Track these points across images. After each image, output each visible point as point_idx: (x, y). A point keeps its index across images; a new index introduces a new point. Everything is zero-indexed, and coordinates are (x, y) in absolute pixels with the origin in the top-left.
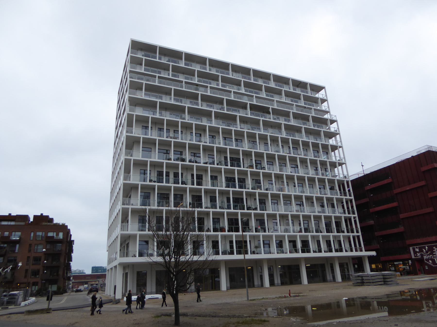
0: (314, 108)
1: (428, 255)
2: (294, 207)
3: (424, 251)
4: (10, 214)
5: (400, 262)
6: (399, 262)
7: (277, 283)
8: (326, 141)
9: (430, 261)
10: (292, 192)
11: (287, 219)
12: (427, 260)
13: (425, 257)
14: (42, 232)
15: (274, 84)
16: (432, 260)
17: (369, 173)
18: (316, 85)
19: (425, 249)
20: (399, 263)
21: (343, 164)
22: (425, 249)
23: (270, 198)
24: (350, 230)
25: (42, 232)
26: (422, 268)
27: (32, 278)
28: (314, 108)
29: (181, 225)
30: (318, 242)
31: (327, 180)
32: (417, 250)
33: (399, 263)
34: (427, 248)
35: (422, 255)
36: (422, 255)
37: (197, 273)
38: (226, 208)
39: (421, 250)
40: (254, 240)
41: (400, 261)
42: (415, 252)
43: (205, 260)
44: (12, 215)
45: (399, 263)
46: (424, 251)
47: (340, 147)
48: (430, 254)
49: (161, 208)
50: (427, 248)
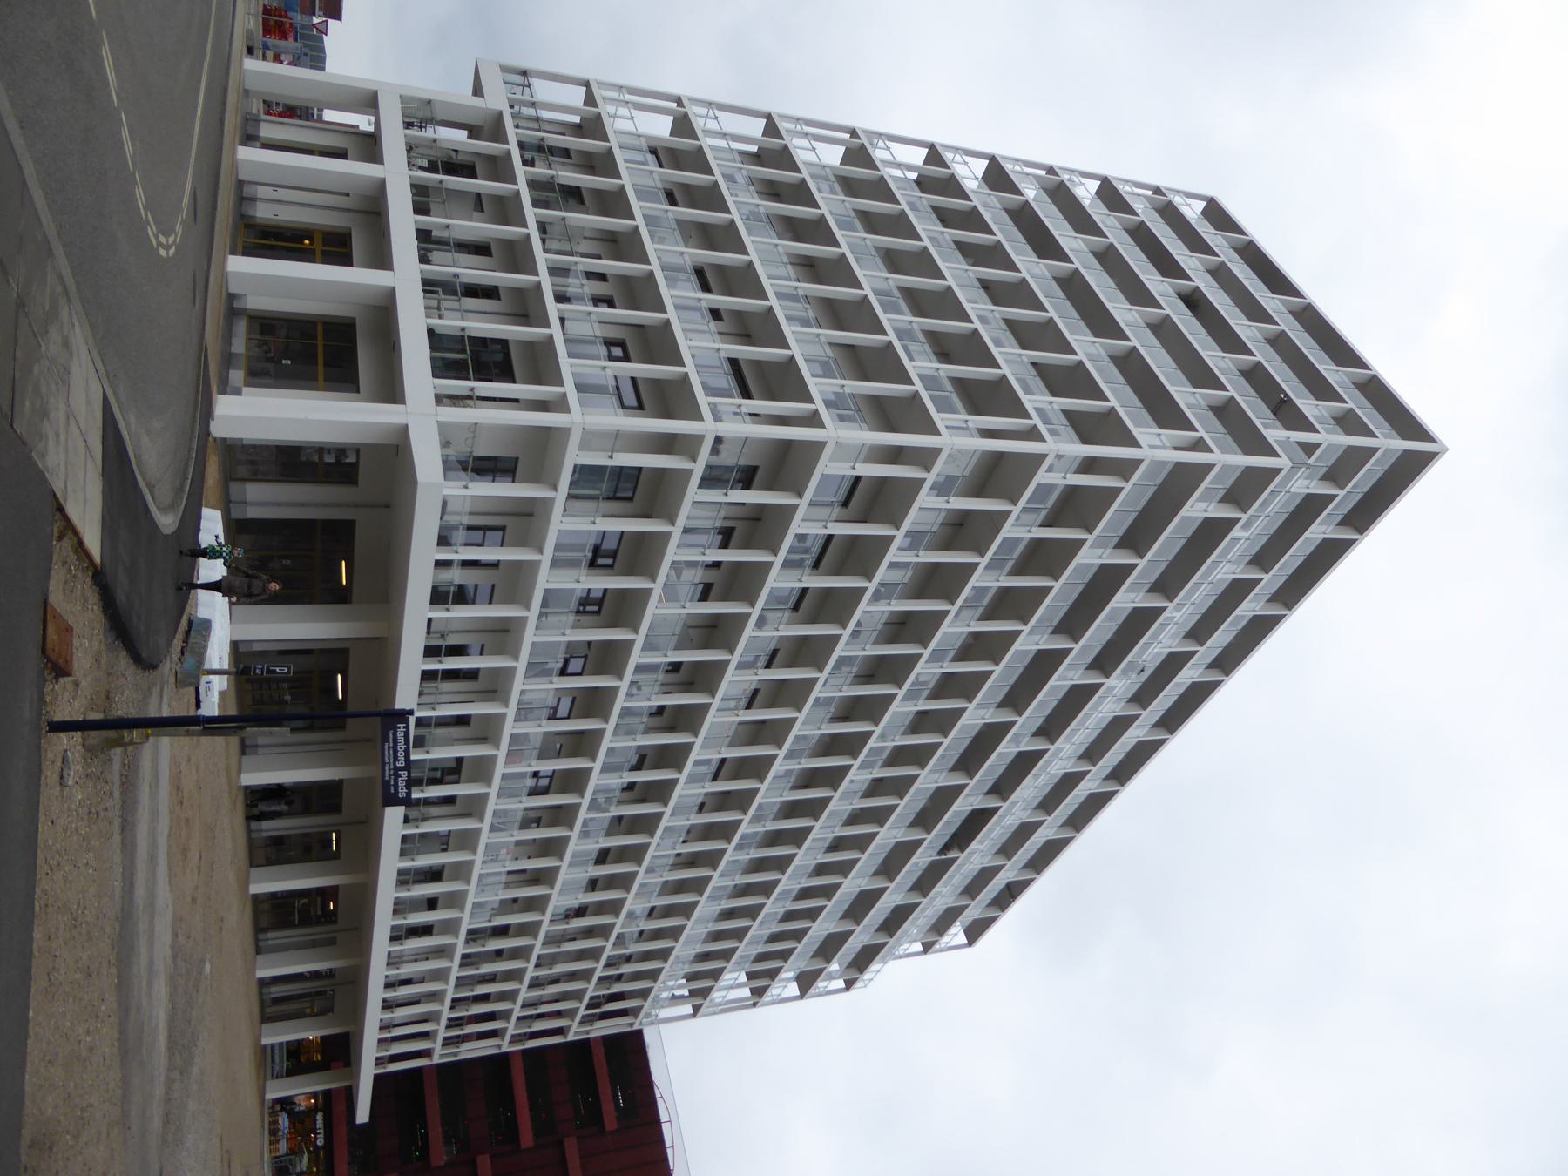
0: (772, 563)
2: (622, 780)
5: (322, 1136)
6: (322, 1131)
7: (260, 741)
8: (472, 634)
10: (722, 699)
11: (485, 649)
15: (530, 136)
18: (1332, 569)
20: (318, 1131)
26: (194, 455)
27: (274, 1123)
28: (772, 563)
29: (164, 894)
31: (546, 895)
33: (319, 1134)
40: (348, 210)
41: (325, 1139)
45: (319, 1134)
47: (696, 1009)
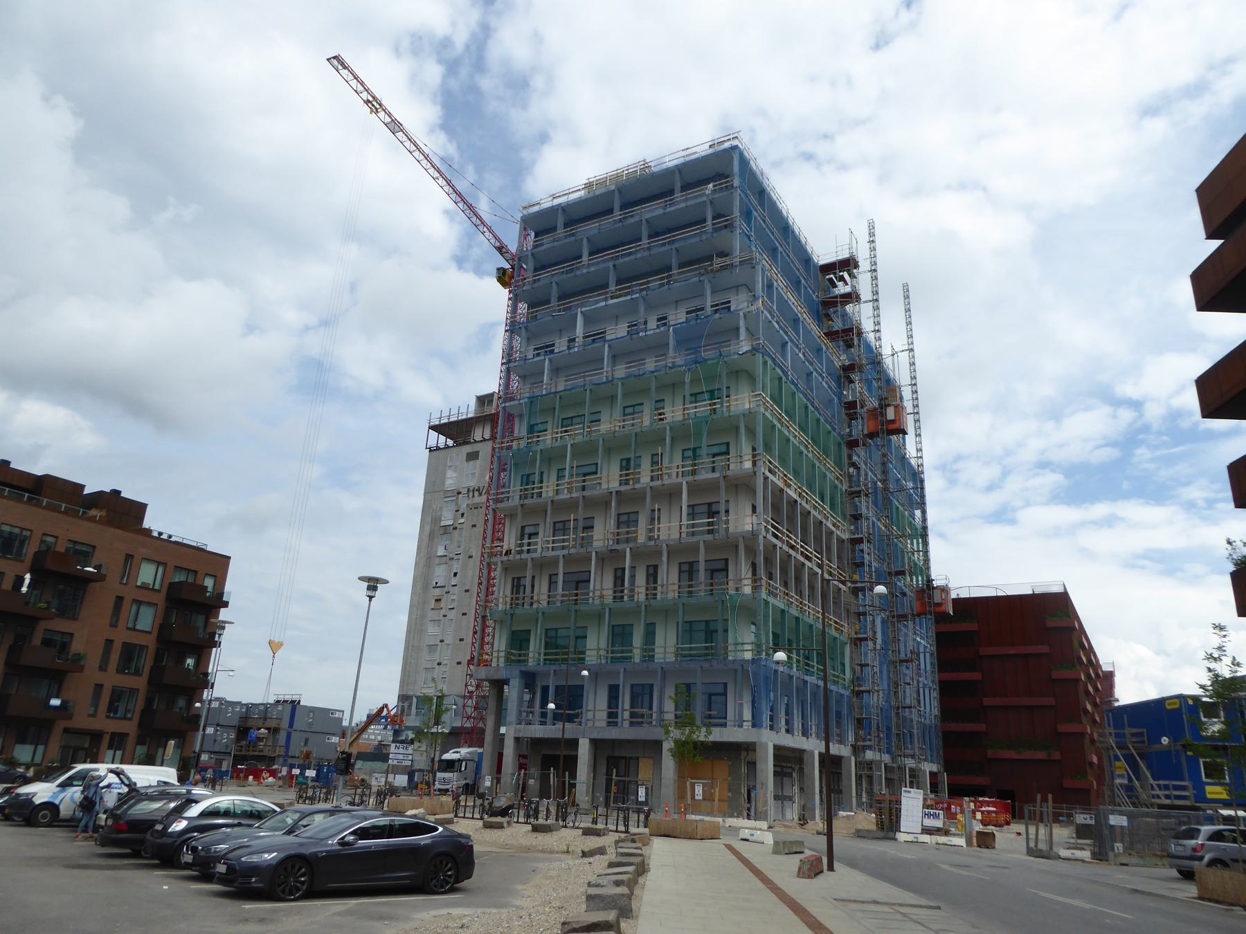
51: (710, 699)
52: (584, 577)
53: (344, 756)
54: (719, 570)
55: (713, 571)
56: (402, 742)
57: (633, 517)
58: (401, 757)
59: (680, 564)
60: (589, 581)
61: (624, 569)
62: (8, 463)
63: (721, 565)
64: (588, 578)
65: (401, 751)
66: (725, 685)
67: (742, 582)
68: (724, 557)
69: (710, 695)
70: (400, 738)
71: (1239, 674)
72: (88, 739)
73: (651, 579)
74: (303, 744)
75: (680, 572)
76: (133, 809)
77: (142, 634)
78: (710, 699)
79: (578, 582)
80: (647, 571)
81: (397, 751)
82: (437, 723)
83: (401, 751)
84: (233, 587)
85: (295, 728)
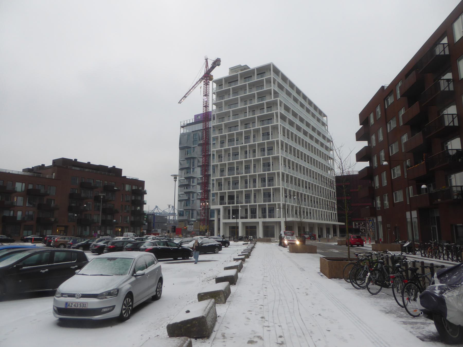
1: (362, 227)
3: (361, 224)
4: (76, 160)
9: (363, 230)
12: (362, 229)
13: (361, 228)
14: (22, 183)
16: (364, 229)
17: (98, 165)
19: (362, 224)
21: (332, 159)
22: (362, 224)
23: (286, 178)
24: (288, 193)
25: (22, 183)
30: (246, 183)
32: (357, 224)
34: (363, 223)
35: (359, 227)
36: (359, 227)
37: (213, 317)
38: (402, 253)
39: (359, 224)
42: (355, 225)
43: (206, 112)
44: (78, 161)
46: (361, 224)
48: (364, 226)
49: (234, 161)
50: (363, 223)
51: (270, 211)
52: (237, 182)
53: (173, 227)
54: (270, 149)
55: (270, 180)
56: (190, 224)
57: (249, 166)
58: (190, 228)
59: (261, 178)
60: (238, 183)
61: (247, 180)
62: (120, 171)
63: (271, 148)
64: (238, 182)
65: (190, 227)
66: (274, 208)
67: (280, 153)
68: (272, 176)
69: (270, 210)
70: (190, 224)
71: (337, 208)
72: (64, 227)
73: (254, 182)
74: (157, 226)
75: (261, 180)
76: (28, 259)
77: (21, 188)
78: (270, 211)
79: (235, 183)
80: (253, 180)
81: (189, 227)
82: (192, 218)
83: (190, 227)
84: (146, 188)
85: (155, 222)
